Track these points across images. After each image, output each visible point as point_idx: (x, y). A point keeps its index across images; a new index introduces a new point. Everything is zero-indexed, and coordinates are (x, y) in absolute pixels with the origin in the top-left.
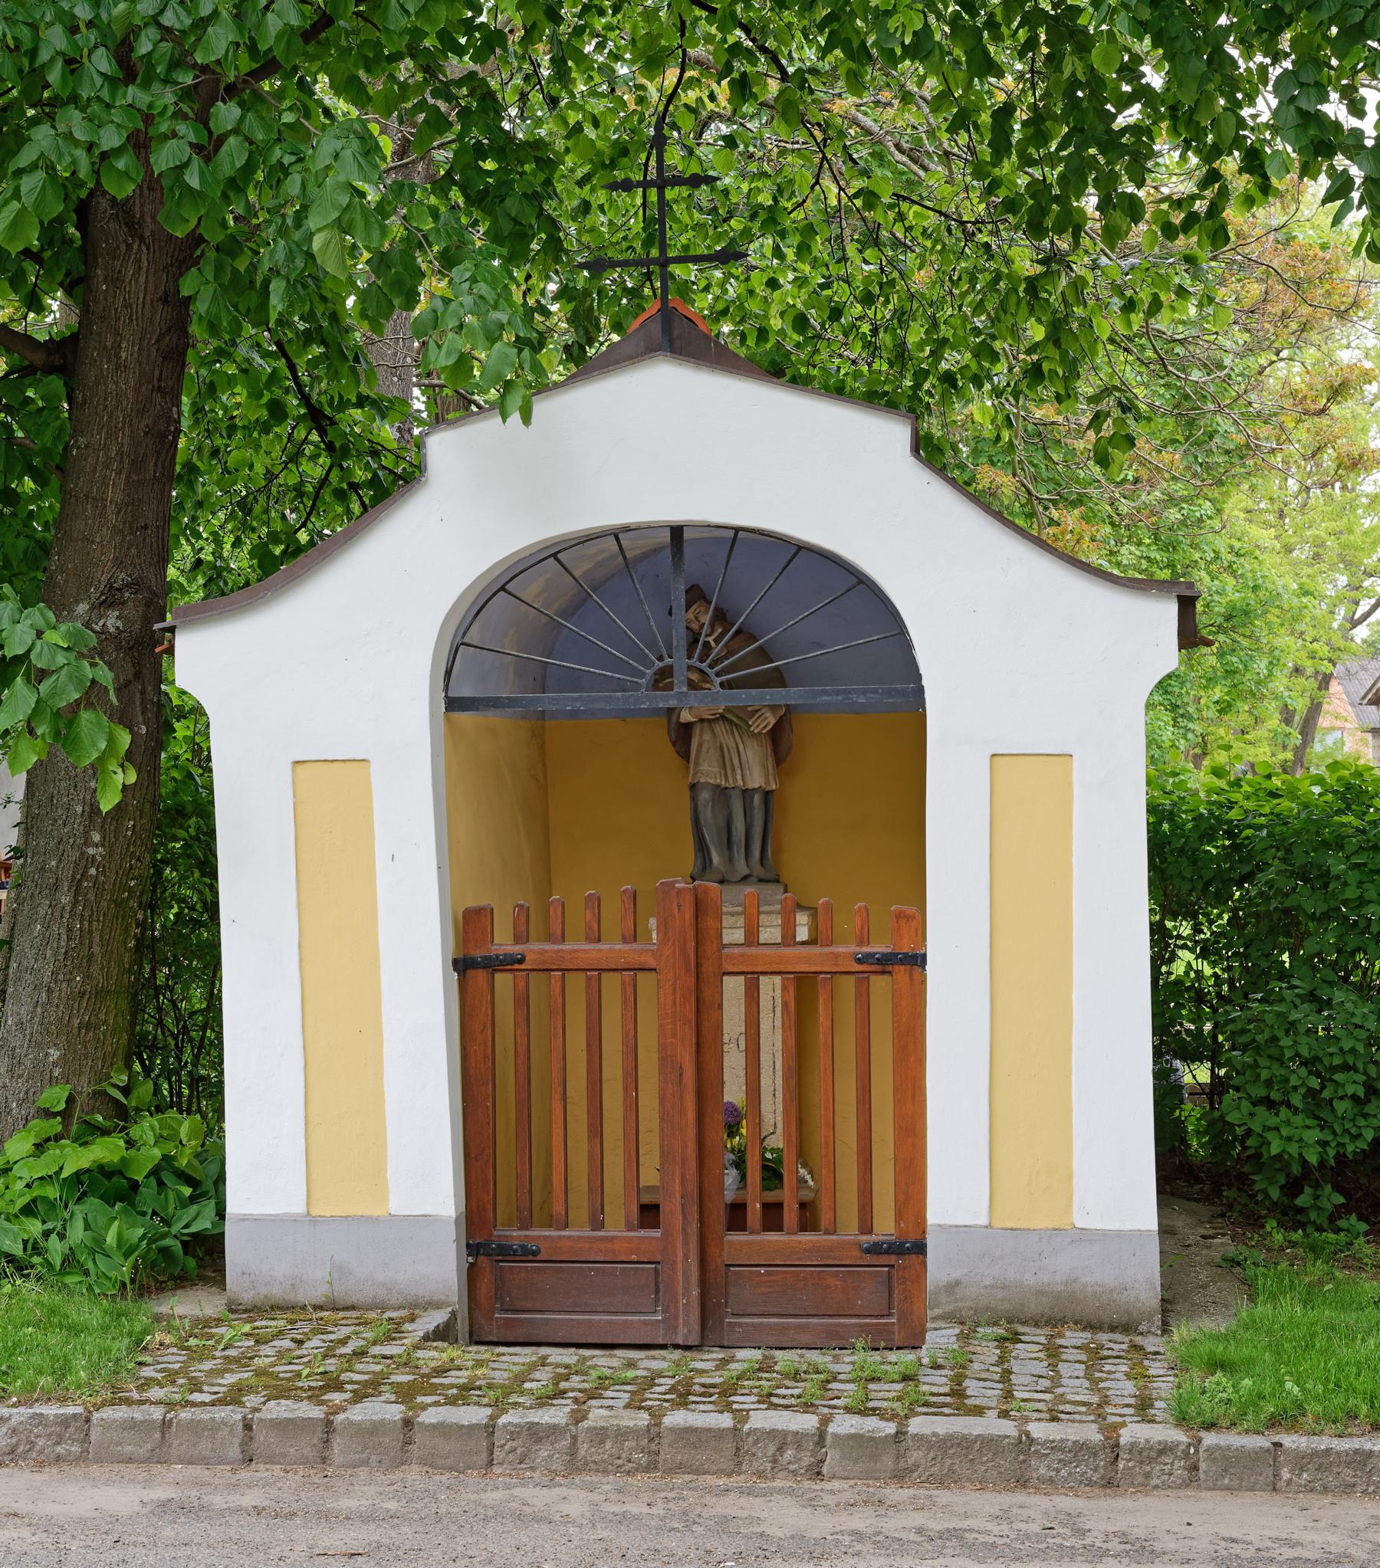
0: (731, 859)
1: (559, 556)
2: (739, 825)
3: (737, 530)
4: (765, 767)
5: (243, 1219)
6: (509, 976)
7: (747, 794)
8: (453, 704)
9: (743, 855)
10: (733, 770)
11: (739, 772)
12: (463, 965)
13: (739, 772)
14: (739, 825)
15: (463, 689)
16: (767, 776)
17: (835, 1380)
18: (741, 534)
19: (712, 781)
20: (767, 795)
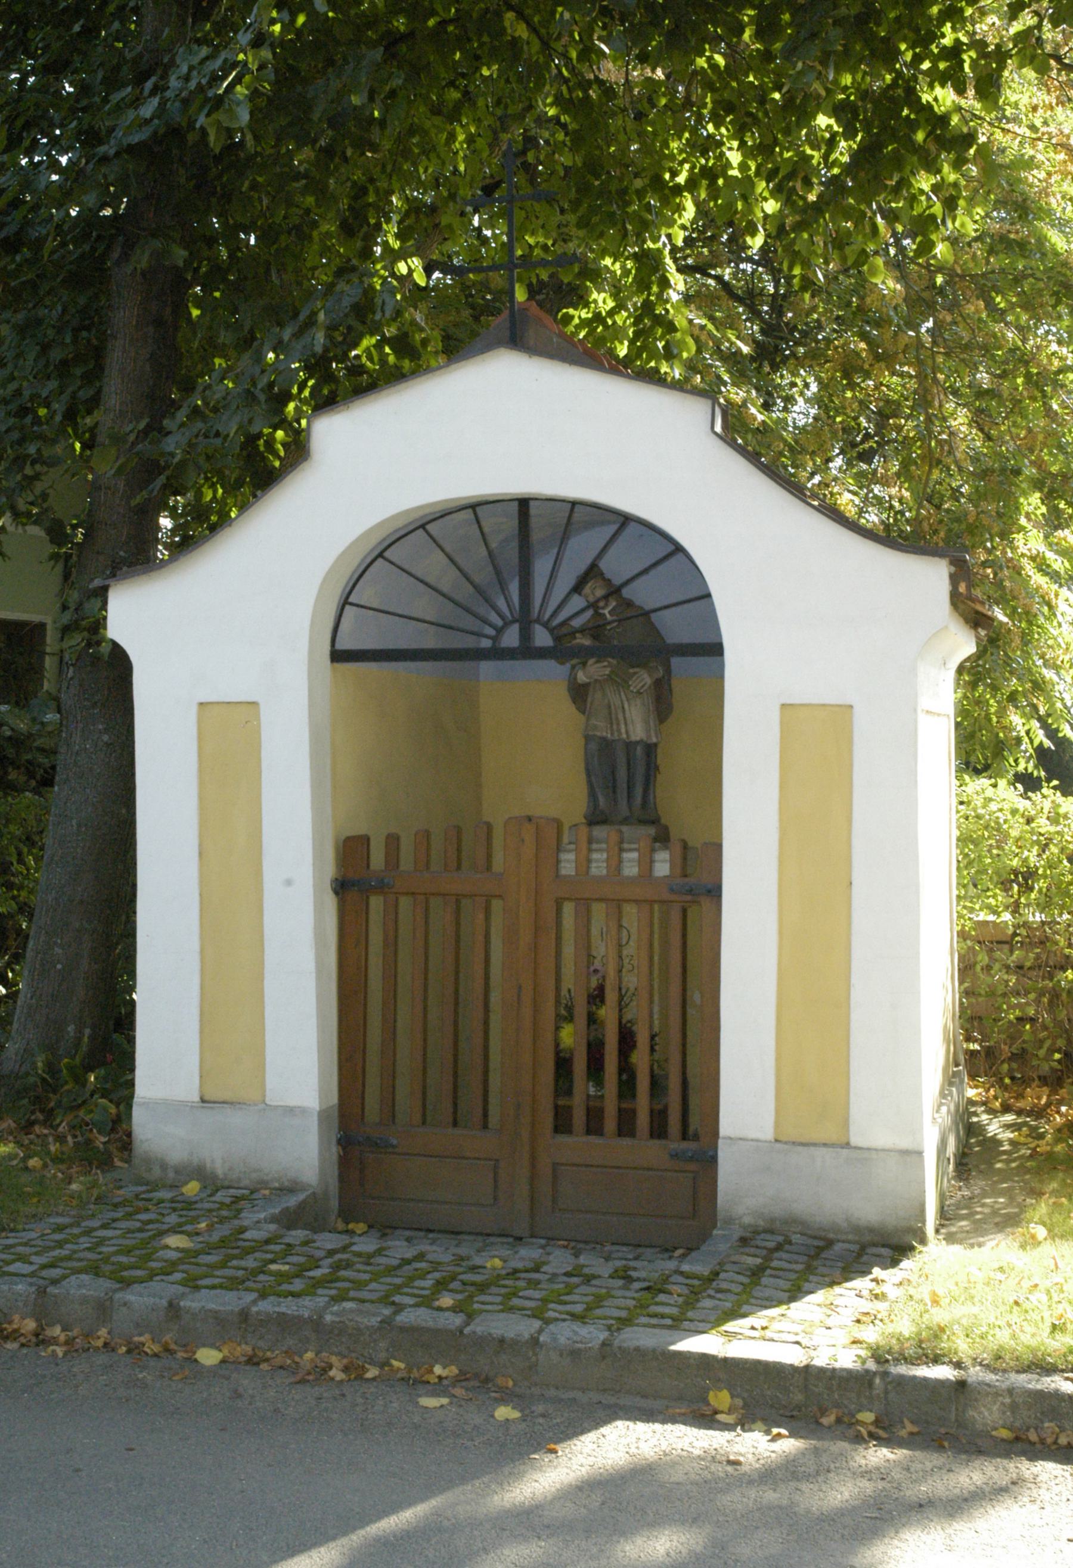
0: (615, 801)
1: (428, 527)
2: (622, 774)
3: (574, 504)
4: (646, 722)
5: (145, 1104)
6: (381, 898)
7: (630, 746)
8: (338, 656)
9: (625, 802)
10: (618, 724)
11: (623, 726)
12: (342, 887)
13: (623, 726)
14: (622, 774)
15: (345, 643)
16: (648, 731)
17: (515, 1295)
18: (577, 508)
19: (598, 734)
20: (650, 749)
